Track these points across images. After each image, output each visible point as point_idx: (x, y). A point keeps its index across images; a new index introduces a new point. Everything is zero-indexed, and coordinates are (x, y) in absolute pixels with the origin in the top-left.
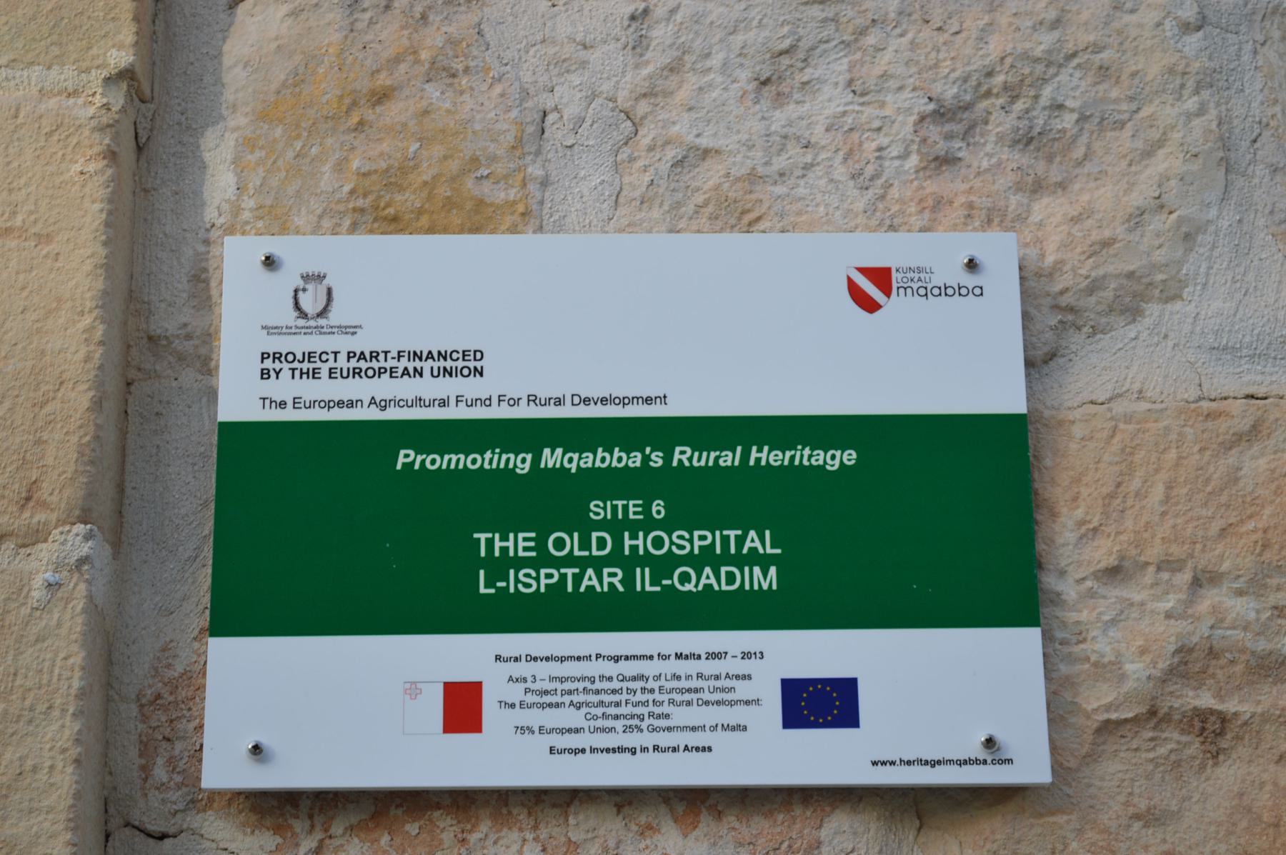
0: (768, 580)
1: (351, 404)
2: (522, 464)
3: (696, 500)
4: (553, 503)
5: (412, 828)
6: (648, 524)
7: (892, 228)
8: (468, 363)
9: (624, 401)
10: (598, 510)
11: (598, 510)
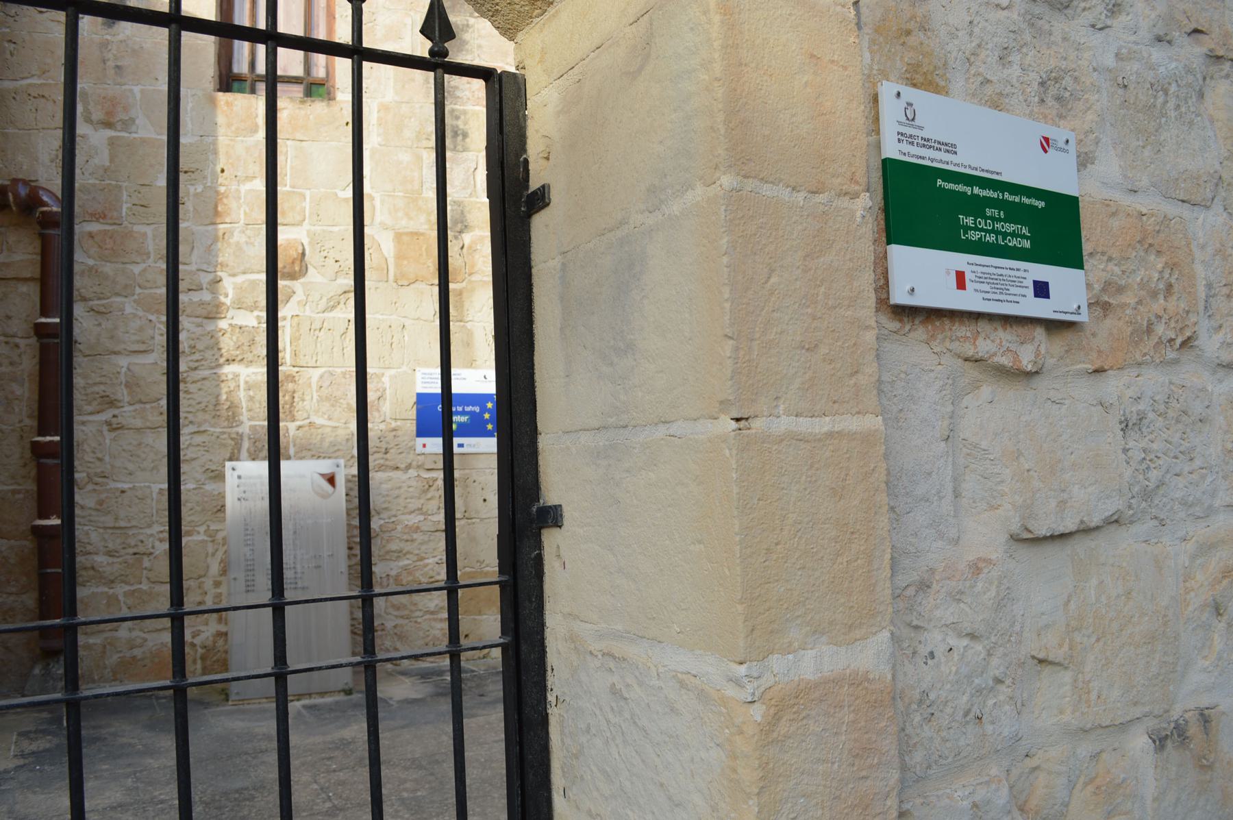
0: (1027, 244)
1: (923, 158)
2: (968, 190)
3: (1015, 213)
4: (977, 207)
5: (938, 324)
6: (1000, 220)
7: (996, 106)
8: (951, 148)
9: (992, 173)
10: (989, 212)
11: (989, 212)
